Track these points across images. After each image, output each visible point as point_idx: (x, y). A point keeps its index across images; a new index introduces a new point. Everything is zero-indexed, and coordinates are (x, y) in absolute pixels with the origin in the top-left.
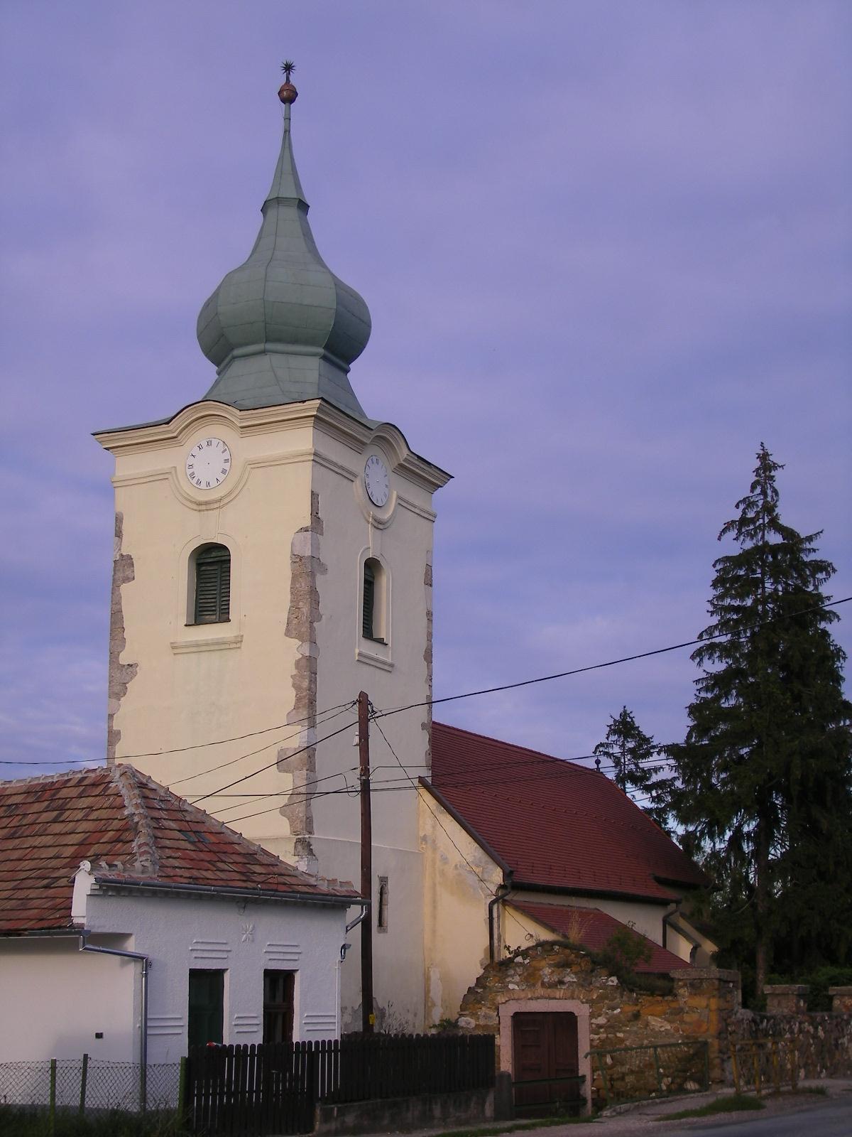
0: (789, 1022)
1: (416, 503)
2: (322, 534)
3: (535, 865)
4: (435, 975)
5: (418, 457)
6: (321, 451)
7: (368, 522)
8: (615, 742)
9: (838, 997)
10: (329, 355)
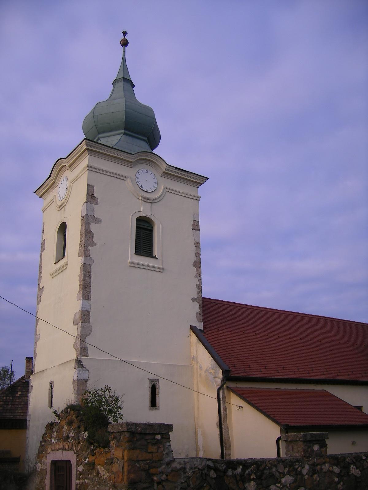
1: (182, 191)
2: (97, 204)
4: (200, 432)
5: (176, 168)
6: (92, 165)
7: (140, 199)
10: (127, 132)
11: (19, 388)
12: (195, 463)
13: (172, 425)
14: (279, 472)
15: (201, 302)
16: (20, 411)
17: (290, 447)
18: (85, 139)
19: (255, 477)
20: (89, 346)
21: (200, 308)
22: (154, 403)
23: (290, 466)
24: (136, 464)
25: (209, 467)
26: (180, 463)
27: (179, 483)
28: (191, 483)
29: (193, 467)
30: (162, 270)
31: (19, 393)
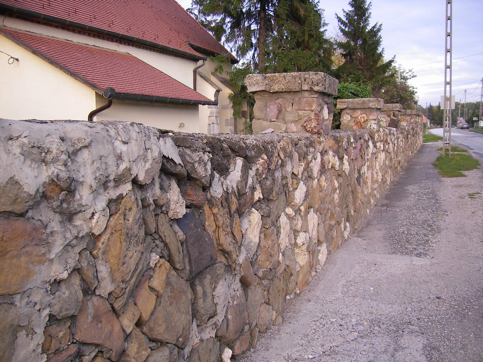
0: (303, 157)
3: (49, 4)
8: (195, 8)
9: (348, 111)
27: (37, 297)
28: (103, 271)
29: (112, 178)
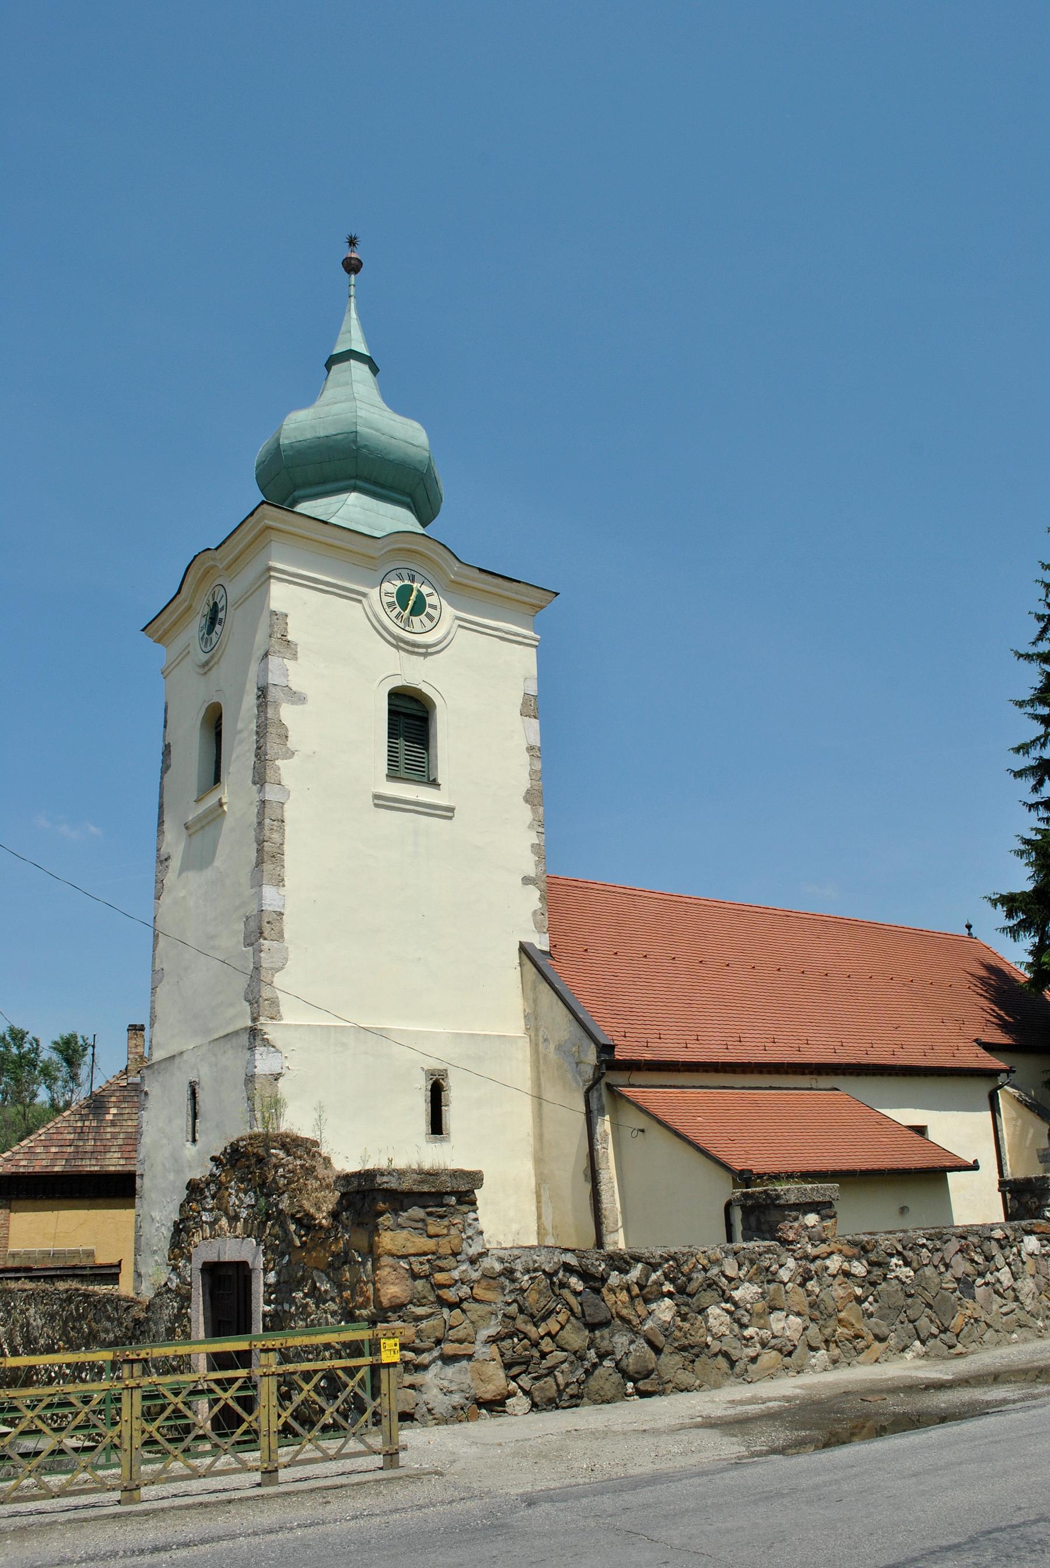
2: (295, 657)
11: (113, 1099)
12: (535, 1257)
13: (480, 1172)
14: (726, 1277)
15: (543, 886)
16: (116, 1155)
17: (753, 1220)
18: (263, 503)
19: (672, 1289)
20: (281, 995)
21: (542, 898)
22: (437, 1126)
23: (752, 1262)
24: (401, 1263)
25: (567, 1268)
26: (501, 1260)
30: (447, 812)
31: (114, 1111)
